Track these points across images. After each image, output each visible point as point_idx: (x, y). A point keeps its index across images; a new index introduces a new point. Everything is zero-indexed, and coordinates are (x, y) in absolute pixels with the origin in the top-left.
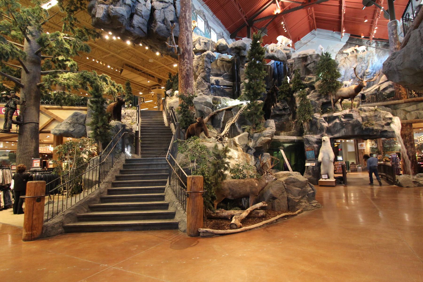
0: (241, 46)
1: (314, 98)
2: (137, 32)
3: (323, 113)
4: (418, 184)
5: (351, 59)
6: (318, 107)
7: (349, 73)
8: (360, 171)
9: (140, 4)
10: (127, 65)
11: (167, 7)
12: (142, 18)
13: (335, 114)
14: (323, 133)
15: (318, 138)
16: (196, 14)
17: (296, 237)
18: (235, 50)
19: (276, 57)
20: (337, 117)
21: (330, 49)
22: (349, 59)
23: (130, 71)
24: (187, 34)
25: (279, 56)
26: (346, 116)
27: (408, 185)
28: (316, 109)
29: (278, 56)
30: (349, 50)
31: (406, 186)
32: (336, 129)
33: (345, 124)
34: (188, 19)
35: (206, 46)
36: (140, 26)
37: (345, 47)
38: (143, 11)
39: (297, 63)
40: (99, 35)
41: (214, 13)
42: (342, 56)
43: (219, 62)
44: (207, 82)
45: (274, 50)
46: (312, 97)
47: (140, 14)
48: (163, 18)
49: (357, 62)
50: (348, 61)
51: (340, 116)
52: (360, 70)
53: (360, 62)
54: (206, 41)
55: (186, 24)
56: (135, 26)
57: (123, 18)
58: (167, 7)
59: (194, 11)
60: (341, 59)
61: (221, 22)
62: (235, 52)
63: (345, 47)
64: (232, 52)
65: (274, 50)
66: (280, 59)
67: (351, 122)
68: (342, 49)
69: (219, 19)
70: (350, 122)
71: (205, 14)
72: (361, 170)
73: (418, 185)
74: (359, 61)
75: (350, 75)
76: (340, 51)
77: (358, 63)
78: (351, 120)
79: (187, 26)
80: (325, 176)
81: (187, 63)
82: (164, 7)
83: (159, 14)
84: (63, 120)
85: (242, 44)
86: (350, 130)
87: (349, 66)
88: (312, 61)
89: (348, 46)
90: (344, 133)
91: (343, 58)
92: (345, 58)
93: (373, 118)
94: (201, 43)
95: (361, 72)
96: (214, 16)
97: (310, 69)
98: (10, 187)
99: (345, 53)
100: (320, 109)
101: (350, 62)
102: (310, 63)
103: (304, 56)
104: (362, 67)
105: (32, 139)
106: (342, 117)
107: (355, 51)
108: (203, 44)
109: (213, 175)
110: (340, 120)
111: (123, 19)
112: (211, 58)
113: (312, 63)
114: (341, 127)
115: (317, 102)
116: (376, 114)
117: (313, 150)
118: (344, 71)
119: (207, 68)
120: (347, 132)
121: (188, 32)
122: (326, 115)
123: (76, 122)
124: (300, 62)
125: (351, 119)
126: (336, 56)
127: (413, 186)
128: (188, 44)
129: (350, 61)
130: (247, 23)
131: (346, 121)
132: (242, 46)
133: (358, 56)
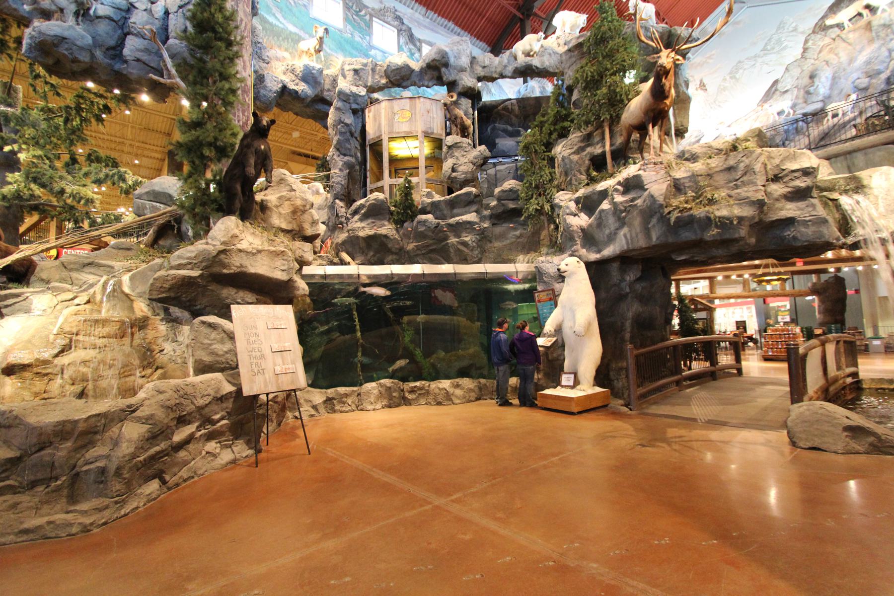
2: (134, 71)
4: (871, 439)
5: (851, 37)
6: (579, 171)
7: (846, 79)
8: (877, 353)
9: (136, 11)
10: (294, 153)
12: (142, 40)
14: (575, 247)
16: (367, 17)
18: (429, 72)
19: (539, 65)
21: (786, 28)
22: (844, 41)
23: (303, 164)
25: (547, 63)
27: (817, 443)
29: (543, 63)
31: (809, 445)
32: (607, 232)
33: (625, 211)
35: (360, 77)
36: (138, 56)
38: (137, 23)
39: (568, 65)
42: (825, 36)
44: (345, 155)
47: (135, 32)
49: (871, 41)
52: (884, 62)
53: (884, 39)
54: (357, 67)
56: (128, 58)
57: (66, 43)
59: (360, 11)
60: (822, 44)
61: (456, 24)
66: (551, 70)
67: (639, 202)
69: (446, 18)
70: (635, 203)
71: (401, 15)
72: (883, 350)
73: (871, 444)
74: (878, 36)
75: (850, 83)
76: (816, 24)
77: (876, 45)
82: (182, 3)
83: (176, 22)
84: (589, 265)
85: (436, 53)
86: (638, 230)
90: (624, 241)
91: (827, 40)
93: (720, 179)
94: (347, 73)
95: (887, 68)
96: (431, 13)
99: (832, 27)
101: (850, 47)
107: (865, 12)
108: (352, 73)
111: (66, 46)
112: (349, 99)
114: (617, 225)
116: (731, 162)
117: (550, 299)
118: (830, 77)
119: (343, 123)
120: (632, 239)
124: (574, 59)
125: (639, 193)
127: (840, 447)
129: (850, 44)
130: (519, 15)
131: (626, 202)
132: (437, 57)
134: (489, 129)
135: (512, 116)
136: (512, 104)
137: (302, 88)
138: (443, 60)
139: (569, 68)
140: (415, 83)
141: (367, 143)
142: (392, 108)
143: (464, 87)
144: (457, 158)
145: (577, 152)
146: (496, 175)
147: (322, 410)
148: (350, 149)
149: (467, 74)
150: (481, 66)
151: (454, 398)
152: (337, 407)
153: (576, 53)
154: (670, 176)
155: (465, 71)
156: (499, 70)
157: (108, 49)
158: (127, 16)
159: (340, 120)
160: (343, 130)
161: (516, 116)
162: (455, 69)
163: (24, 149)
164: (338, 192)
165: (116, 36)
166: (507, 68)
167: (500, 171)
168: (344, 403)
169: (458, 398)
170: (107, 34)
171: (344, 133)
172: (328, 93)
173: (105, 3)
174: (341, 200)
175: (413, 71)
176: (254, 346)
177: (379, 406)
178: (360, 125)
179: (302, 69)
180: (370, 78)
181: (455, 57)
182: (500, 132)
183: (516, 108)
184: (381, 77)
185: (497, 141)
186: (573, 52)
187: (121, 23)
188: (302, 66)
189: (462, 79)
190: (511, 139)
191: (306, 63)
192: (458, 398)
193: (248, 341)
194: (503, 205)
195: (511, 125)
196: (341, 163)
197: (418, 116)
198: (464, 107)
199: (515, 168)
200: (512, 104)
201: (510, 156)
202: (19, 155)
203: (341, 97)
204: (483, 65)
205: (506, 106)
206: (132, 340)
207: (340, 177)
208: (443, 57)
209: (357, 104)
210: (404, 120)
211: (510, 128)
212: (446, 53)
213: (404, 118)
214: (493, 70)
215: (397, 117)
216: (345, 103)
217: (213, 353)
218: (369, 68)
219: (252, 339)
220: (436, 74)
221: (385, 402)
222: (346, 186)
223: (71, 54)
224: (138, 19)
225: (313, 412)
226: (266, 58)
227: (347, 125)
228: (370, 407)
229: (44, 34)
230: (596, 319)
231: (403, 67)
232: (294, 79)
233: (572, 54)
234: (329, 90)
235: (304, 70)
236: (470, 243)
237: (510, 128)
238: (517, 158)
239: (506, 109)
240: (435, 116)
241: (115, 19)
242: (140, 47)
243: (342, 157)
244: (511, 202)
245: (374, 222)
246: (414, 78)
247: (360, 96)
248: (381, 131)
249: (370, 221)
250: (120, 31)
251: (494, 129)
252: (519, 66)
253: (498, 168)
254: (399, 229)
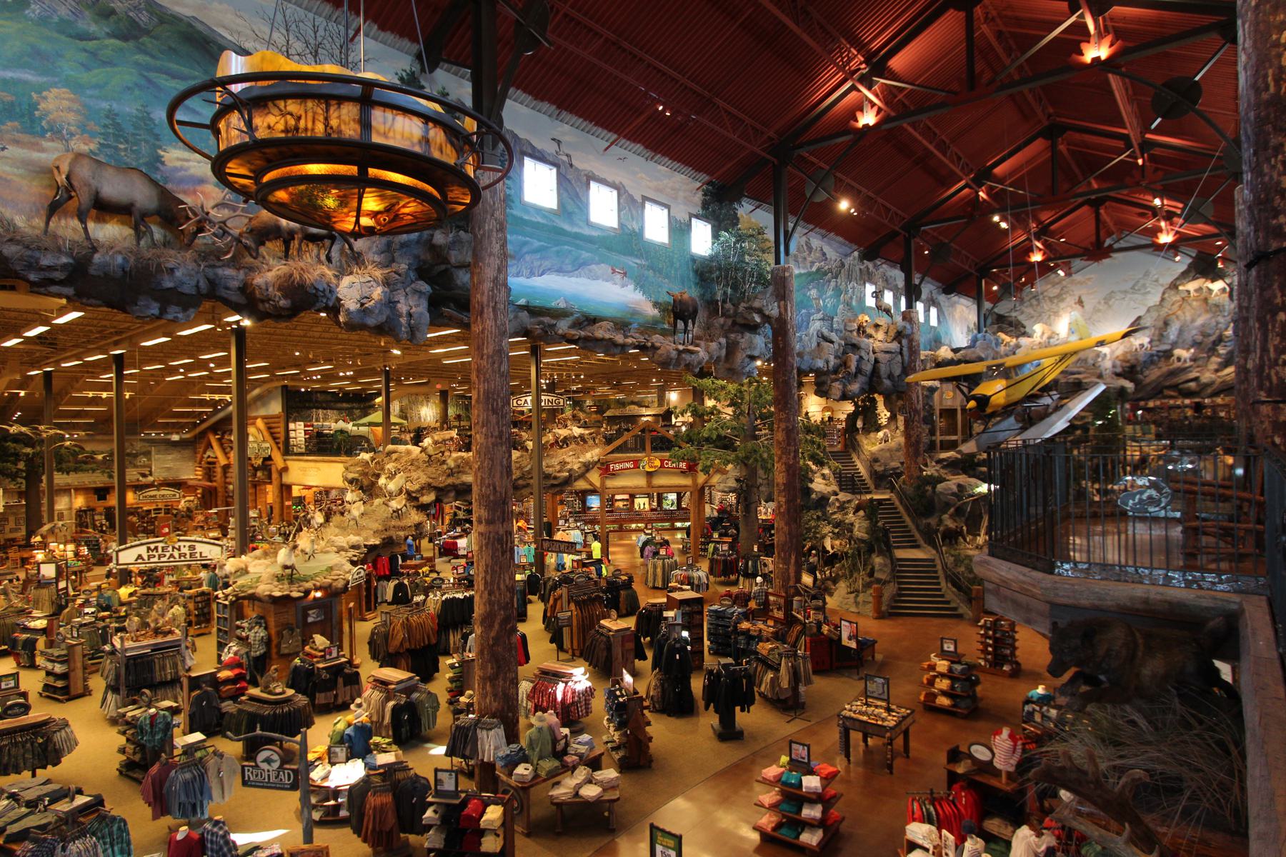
3: (1093, 483)
17: (319, 594)
30: (1192, 286)
37: (1185, 276)
40: (458, 701)
41: (558, 107)
45: (658, 348)
49: (1207, 311)
50: (1188, 308)
63: (1185, 276)
65: (658, 348)
68: (1177, 279)
87: (1188, 318)
89: (1192, 274)
92: (1183, 299)
98: (891, 293)
104: (1218, 323)
109: (1066, 741)
126: (1164, 293)
133: (1210, 301)
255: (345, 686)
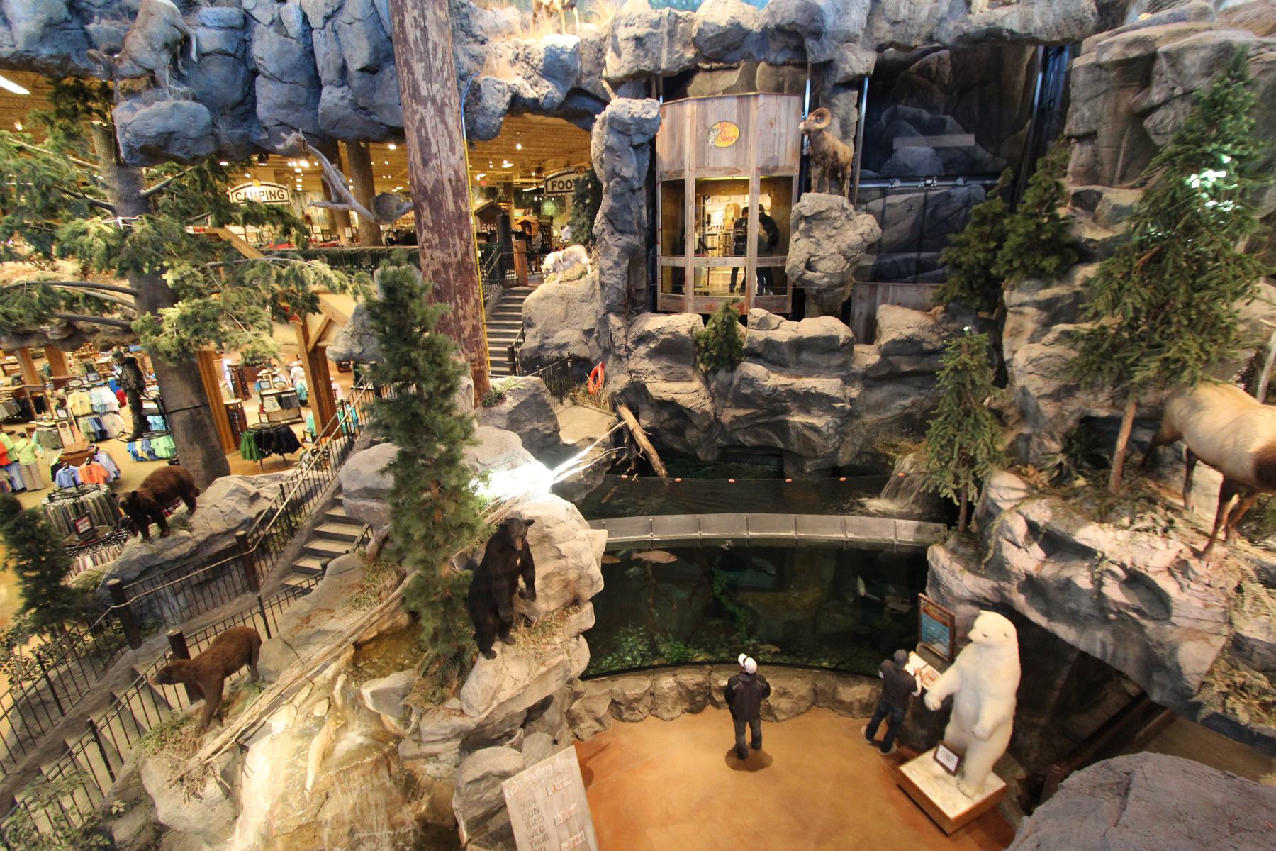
0: (793, 23)
1: (1047, 374)
3: (1033, 492)
11: (339, 8)
12: (279, 85)
13: (1091, 534)
15: (978, 591)
20: (1086, 553)
24: (418, 117)
26: (1135, 580)
28: (1035, 439)
29: (1027, 21)
34: (416, 42)
36: (281, 119)
39: (1086, 94)
43: (763, 72)
44: (622, 232)
46: (1038, 366)
48: (340, 61)
51: (1104, 565)
54: (641, 32)
55: (411, 71)
58: (339, 8)
62: (786, 46)
64: (773, 46)
67: (1149, 625)
70: (1143, 622)
78: (1153, 619)
79: (414, 80)
80: (948, 758)
81: (430, 247)
82: (329, 11)
85: (798, 9)
88: (1178, 91)
94: (622, 45)
97: (1158, 141)
100: (1055, 446)
102: (1166, 103)
103: (1135, 53)
105: (191, 443)
106: (1113, 574)
108: (632, 44)
110: (1099, 583)
113: (1177, 104)
115: (1048, 409)
119: (618, 175)
121: (421, 108)
122: (1041, 512)
123: (362, 331)
124: (1104, 86)
128: (425, 163)
131: (1126, 606)
134: (884, 116)
135: (935, 88)
136: (939, 59)
137: (545, 91)
138: (812, 27)
139: (1086, 101)
140: (750, 54)
141: (658, 179)
142: (704, 117)
143: (847, 75)
144: (818, 243)
145: (1056, 396)
146: (884, 211)
147: (611, 721)
148: (630, 223)
149: (858, 46)
150: (889, 20)
151: (777, 714)
152: (626, 716)
153: (1113, 74)
154: (1230, 623)
155: (854, 42)
156: (925, 31)
157: (232, 109)
158: (246, 37)
159: (613, 170)
160: (619, 190)
161: (945, 89)
162: (834, 38)
163: (167, 268)
164: (613, 302)
165: (239, 82)
166: (945, 24)
167: (893, 205)
168: (633, 709)
169: (783, 712)
170: (226, 81)
171: (622, 195)
172: (588, 80)
173: (209, 24)
174: (617, 314)
175: (747, 33)
176: (536, 827)
177: (677, 712)
178: (647, 163)
179: (542, 56)
180: (665, 52)
181: (838, 11)
182: (905, 123)
183: (947, 69)
184: (685, 45)
185: (898, 143)
186: (1107, 70)
187: (239, 55)
188: (542, 51)
189: (845, 61)
190: (922, 139)
191: (549, 44)
192: (783, 712)
193: (528, 825)
194: (890, 363)
195: (930, 109)
196: (617, 251)
197: (752, 136)
198: (841, 112)
199: (921, 201)
200: (939, 59)
201: (916, 179)
202: (165, 277)
203: (616, 125)
204: (894, 18)
205: (927, 64)
206: (389, 769)
207: (615, 275)
208: (813, 20)
209: (643, 134)
210: (726, 144)
211: (926, 115)
212: (820, 11)
213: (725, 139)
214: (914, 32)
215: (712, 136)
216: (622, 137)
217: (483, 804)
218: (664, 30)
219: (532, 819)
220: (793, 42)
221: (686, 706)
222: (624, 290)
223: (188, 153)
224: (265, 47)
225: (597, 727)
226: (479, 32)
227: (624, 179)
228: (666, 716)
229: (143, 136)
230: (1011, 721)
231: (729, 30)
232: (530, 74)
233: (1104, 74)
234: (590, 74)
235: (546, 57)
236: (824, 430)
237: (926, 115)
238: (929, 182)
239: (925, 71)
240: (783, 131)
241: (231, 51)
242: (280, 100)
243: (618, 235)
244: (906, 358)
245: (670, 368)
246: (750, 47)
247: (648, 120)
248: (682, 163)
249: (664, 363)
250: (242, 70)
251: (894, 116)
252: (972, 30)
253: (891, 199)
254: (710, 377)
255: (1041, 306)
